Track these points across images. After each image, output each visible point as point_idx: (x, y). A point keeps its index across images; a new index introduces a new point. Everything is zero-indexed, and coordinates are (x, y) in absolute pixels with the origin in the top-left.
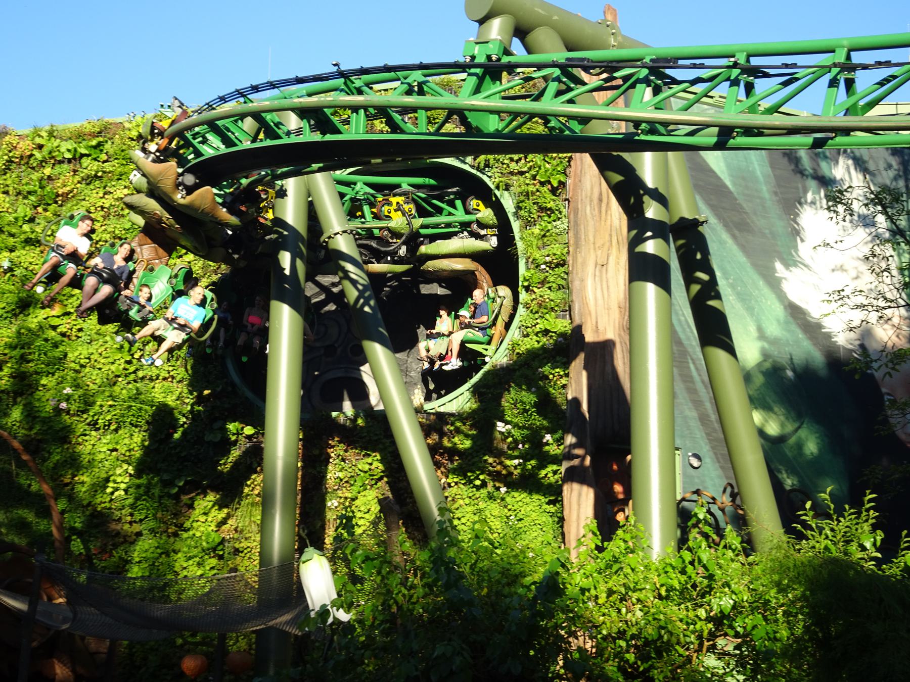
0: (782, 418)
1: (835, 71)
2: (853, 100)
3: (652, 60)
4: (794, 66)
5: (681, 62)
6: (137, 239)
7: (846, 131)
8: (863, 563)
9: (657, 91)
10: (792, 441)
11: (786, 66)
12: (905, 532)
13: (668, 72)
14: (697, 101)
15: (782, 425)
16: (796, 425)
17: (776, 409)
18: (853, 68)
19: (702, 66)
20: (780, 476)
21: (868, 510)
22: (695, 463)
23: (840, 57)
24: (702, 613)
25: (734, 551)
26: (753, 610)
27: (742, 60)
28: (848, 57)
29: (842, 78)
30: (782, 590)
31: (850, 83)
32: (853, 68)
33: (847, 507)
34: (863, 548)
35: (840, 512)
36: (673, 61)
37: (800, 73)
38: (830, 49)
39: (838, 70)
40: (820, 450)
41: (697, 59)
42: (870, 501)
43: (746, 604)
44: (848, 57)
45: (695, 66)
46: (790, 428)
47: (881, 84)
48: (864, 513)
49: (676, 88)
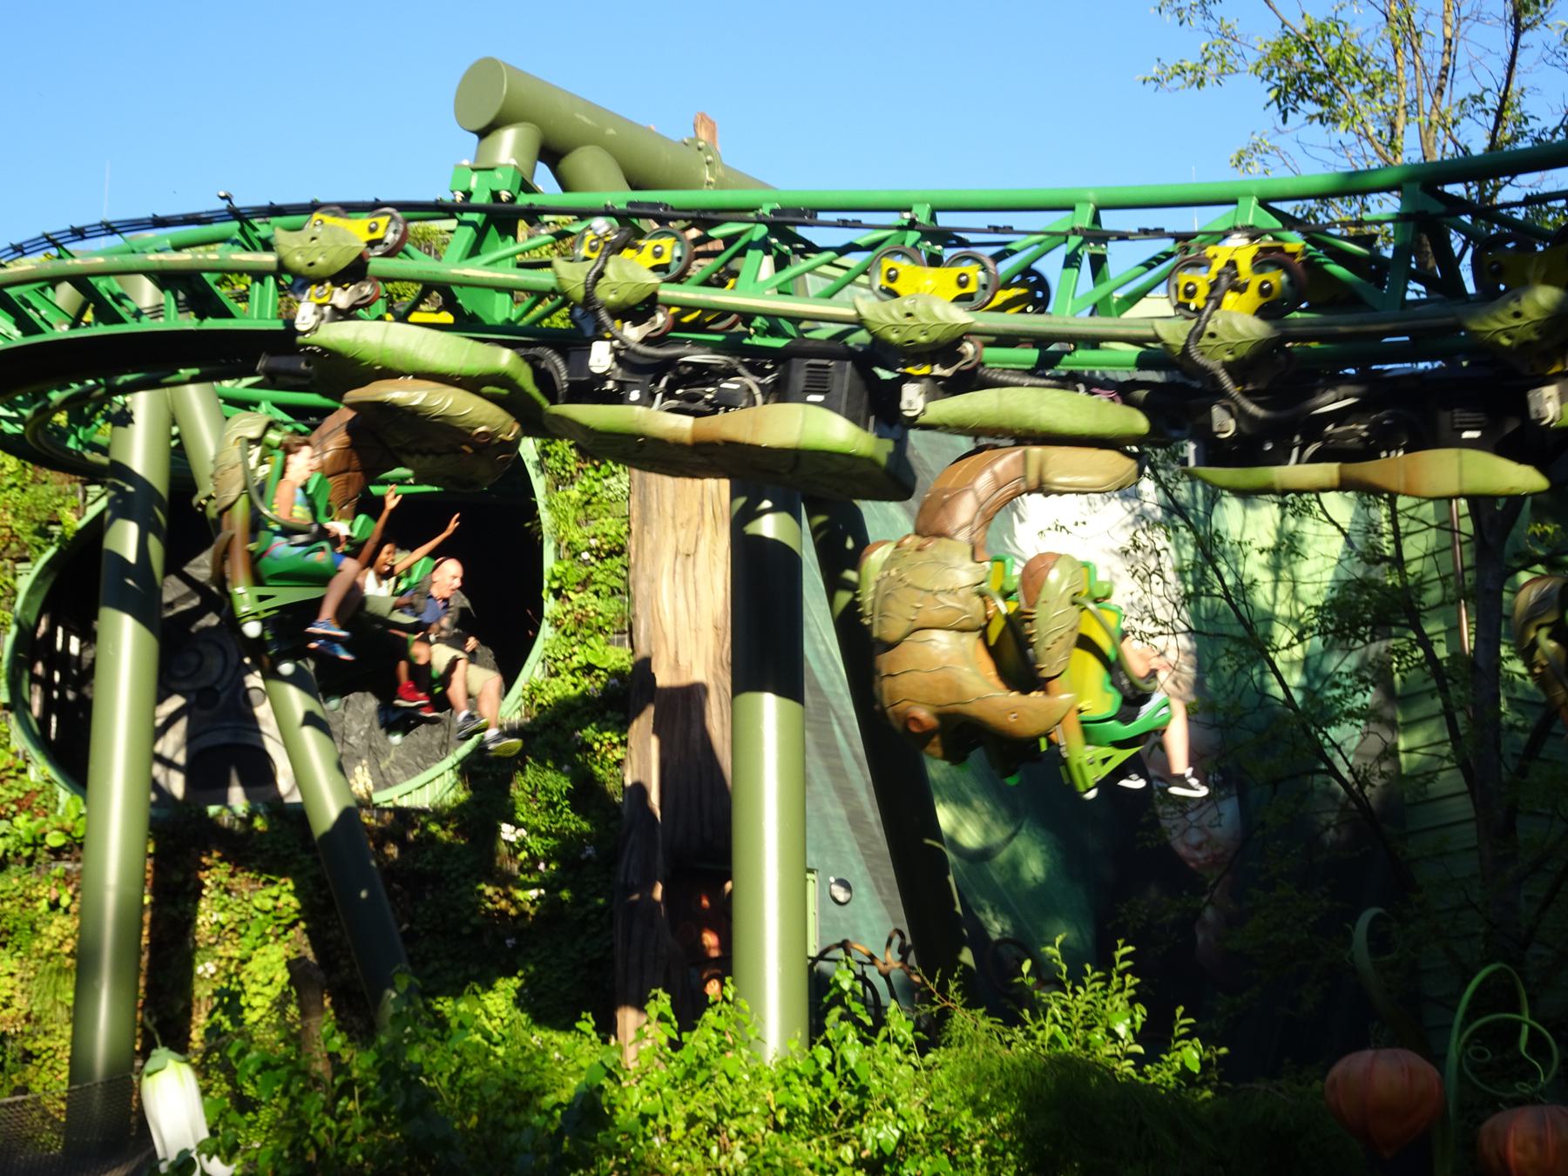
0: (986, 818)
1: (1074, 241)
2: (1103, 289)
3: (773, 211)
4: (1008, 230)
5: (821, 216)
6: (1144, 820)
7: (1094, 342)
8: (1114, 1063)
9: (781, 263)
10: (1002, 857)
11: (996, 230)
12: (1180, 1010)
13: (801, 231)
14: (851, 281)
15: (987, 830)
16: (1010, 830)
17: (976, 803)
18: (1103, 238)
19: (857, 225)
20: (982, 917)
21: (1122, 974)
22: (841, 895)
23: (1083, 219)
24: (847, 1153)
25: (901, 1045)
26: (933, 1146)
27: (923, 218)
28: (1096, 219)
29: (1085, 254)
30: (981, 1112)
31: (1098, 263)
32: (1103, 238)
33: (1088, 968)
34: (1115, 1037)
35: (1077, 977)
36: (807, 215)
37: (1018, 242)
38: (1066, 204)
39: (1079, 239)
40: (1048, 873)
41: (849, 212)
42: (1124, 958)
43: (921, 1136)
44: (1096, 219)
45: (844, 224)
46: (998, 835)
47: (1149, 265)
48: (1116, 980)
49: (815, 259)
